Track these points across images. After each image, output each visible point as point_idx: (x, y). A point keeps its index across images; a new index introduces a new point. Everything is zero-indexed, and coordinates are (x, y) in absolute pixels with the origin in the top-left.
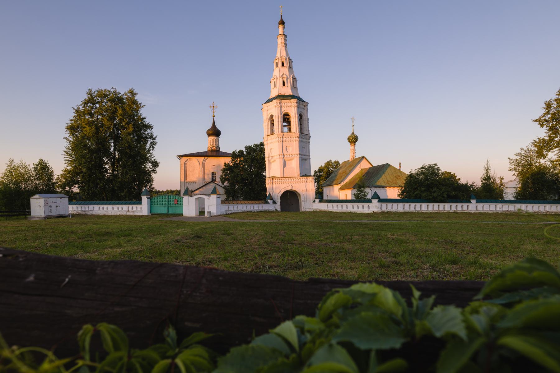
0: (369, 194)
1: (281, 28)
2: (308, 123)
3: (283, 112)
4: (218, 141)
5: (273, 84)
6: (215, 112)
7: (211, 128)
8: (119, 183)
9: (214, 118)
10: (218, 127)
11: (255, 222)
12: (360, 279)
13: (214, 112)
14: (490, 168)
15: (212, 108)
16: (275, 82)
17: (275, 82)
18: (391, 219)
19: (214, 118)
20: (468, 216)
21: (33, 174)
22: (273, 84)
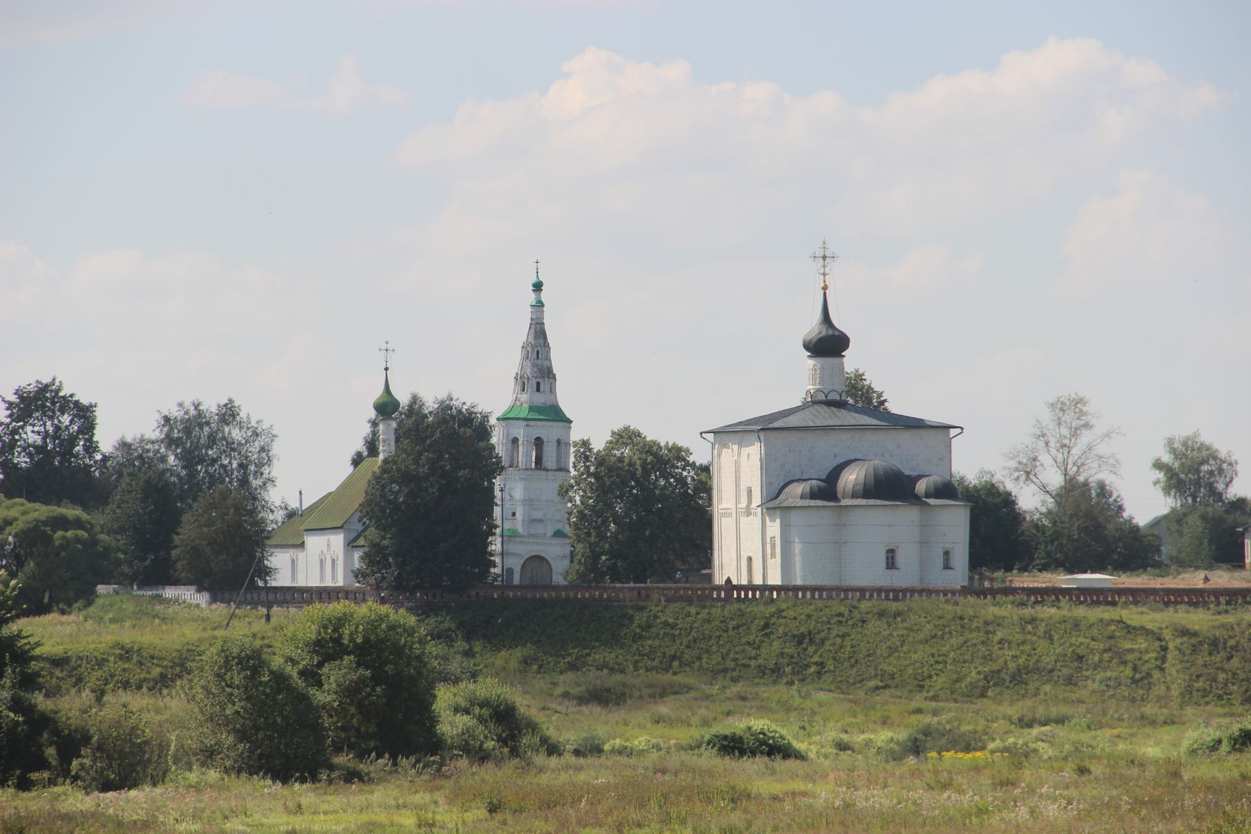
13: (824, 274)
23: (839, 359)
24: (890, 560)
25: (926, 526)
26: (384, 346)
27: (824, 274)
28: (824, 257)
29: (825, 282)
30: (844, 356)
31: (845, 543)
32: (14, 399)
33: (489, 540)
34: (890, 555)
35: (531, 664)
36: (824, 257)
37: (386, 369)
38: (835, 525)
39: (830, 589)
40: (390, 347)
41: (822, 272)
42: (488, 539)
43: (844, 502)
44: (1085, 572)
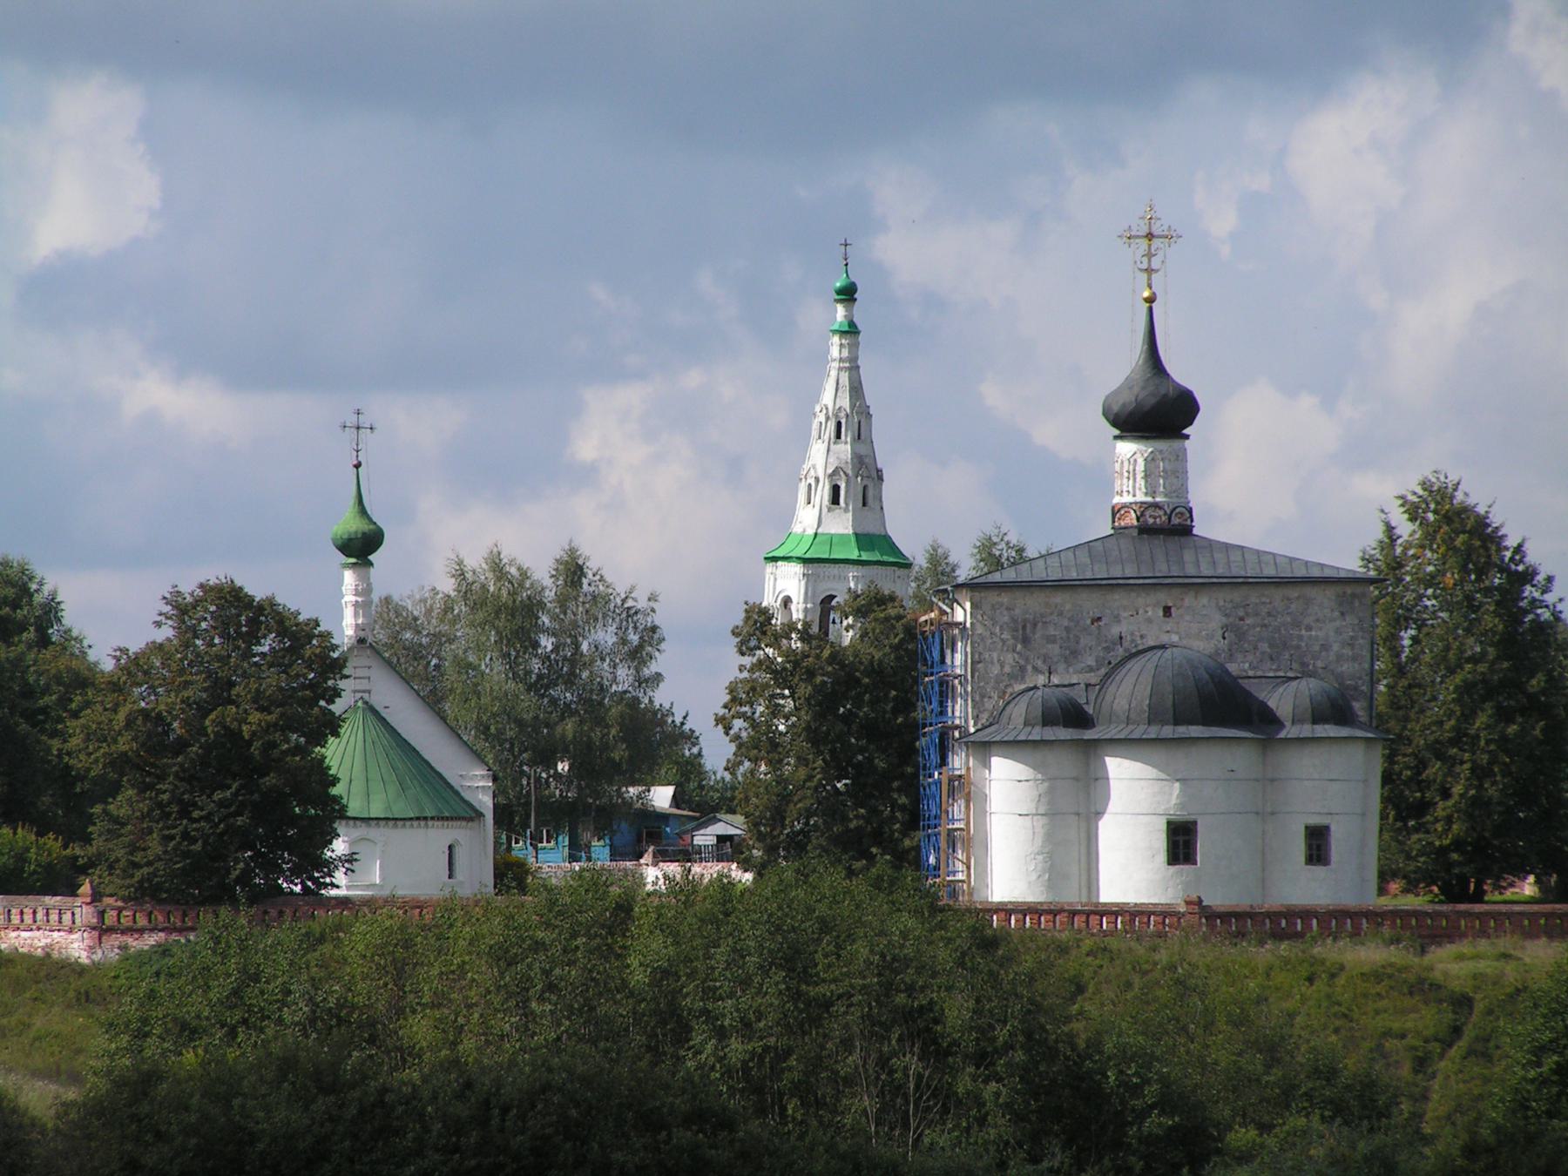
0: (714, 723)
1: (841, 311)
2: (882, 508)
3: (780, 592)
4: (1174, 473)
5: (802, 497)
6: (1157, 271)
7: (1178, 385)
8: (243, 791)
9: (1151, 310)
10: (1181, 371)
11: (684, 810)
12: (211, 827)
13: (1149, 271)
14: (939, 550)
15: (1156, 243)
16: (810, 485)
17: (810, 485)
18: (944, 688)
19: (1151, 310)
20: (513, 845)
21: (1528, 1092)
22: (802, 497)
23: (1176, 444)
24: (1315, 852)
25: (1272, 780)
26: (351, 420)
27: (1149, 271)
28: (1150, 236)
29: (1150, 287)
30: (1187, 437)
31: (1273, 813)
32: (1500, 534)
33: (89, 830)
34: (1181, 839)
35: (1118, 1086)
36: (1150, 236)
37: (357, 466)
38: (1257, 780)
39: (1239, 916)
40: (365, 420)
41: (1145, 266)
42: (88, 828)
43: (1290, 731)
44: (380, 870)
